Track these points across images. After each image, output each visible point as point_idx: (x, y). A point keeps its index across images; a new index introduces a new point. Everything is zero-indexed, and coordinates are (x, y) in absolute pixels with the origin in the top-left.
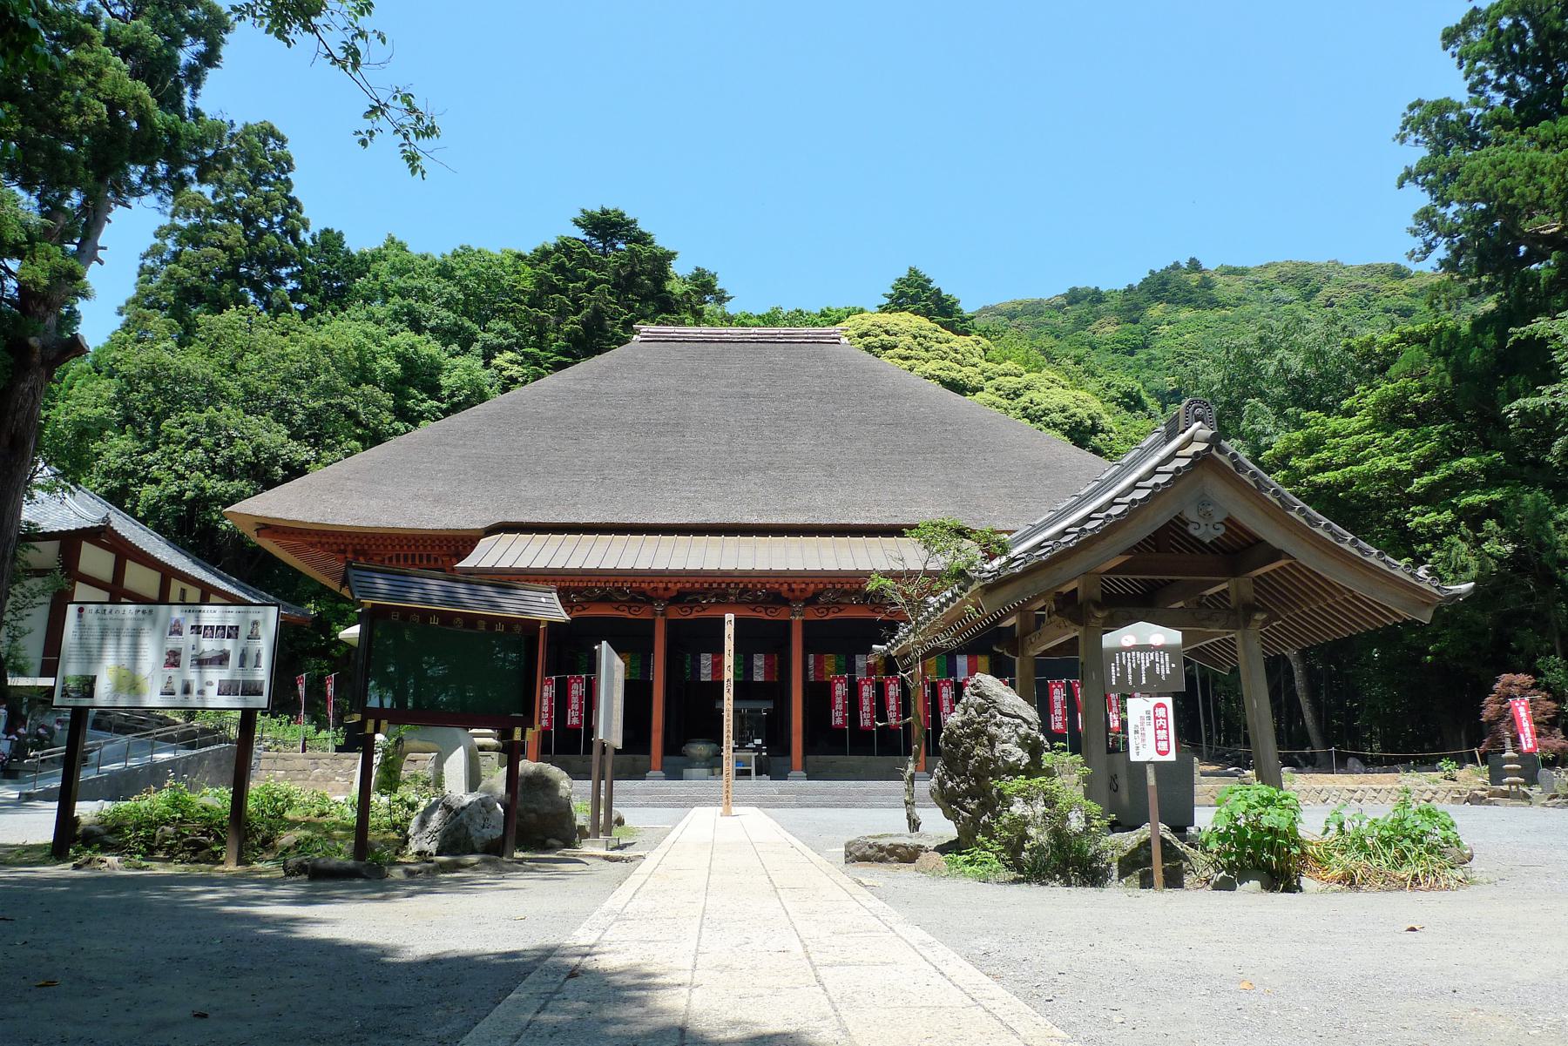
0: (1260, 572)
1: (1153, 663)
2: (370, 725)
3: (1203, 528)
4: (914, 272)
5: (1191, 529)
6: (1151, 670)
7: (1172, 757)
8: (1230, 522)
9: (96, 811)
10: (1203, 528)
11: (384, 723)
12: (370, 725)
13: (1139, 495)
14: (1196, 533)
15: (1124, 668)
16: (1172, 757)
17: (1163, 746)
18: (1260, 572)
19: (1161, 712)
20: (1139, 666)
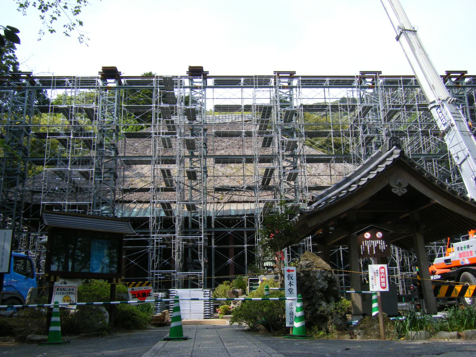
0: (422, 208)
1: (378, 245)
2: (52, 278)
3: (398, 190)
4: (103, 67)
5: (393, 190)
6: (377, 248)
7: (387, 289)
8: (409, 187)
9: (340, 96)
10: (398, 190)
11: (58, 277)
12: (52, 278)
13: (371, 176)
14: (395, 192)
15: (366, 247)
16: (387, 289)
17: (383, 285)
18: (422, 208)
19: (382, 270)
20: (372, 246)
